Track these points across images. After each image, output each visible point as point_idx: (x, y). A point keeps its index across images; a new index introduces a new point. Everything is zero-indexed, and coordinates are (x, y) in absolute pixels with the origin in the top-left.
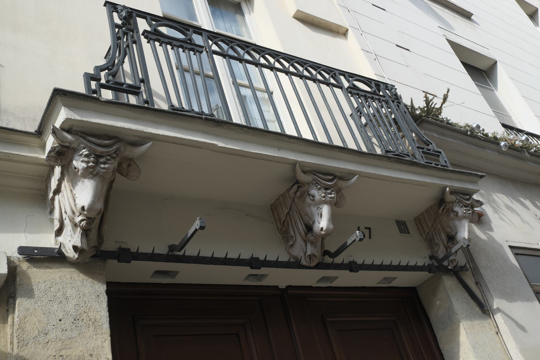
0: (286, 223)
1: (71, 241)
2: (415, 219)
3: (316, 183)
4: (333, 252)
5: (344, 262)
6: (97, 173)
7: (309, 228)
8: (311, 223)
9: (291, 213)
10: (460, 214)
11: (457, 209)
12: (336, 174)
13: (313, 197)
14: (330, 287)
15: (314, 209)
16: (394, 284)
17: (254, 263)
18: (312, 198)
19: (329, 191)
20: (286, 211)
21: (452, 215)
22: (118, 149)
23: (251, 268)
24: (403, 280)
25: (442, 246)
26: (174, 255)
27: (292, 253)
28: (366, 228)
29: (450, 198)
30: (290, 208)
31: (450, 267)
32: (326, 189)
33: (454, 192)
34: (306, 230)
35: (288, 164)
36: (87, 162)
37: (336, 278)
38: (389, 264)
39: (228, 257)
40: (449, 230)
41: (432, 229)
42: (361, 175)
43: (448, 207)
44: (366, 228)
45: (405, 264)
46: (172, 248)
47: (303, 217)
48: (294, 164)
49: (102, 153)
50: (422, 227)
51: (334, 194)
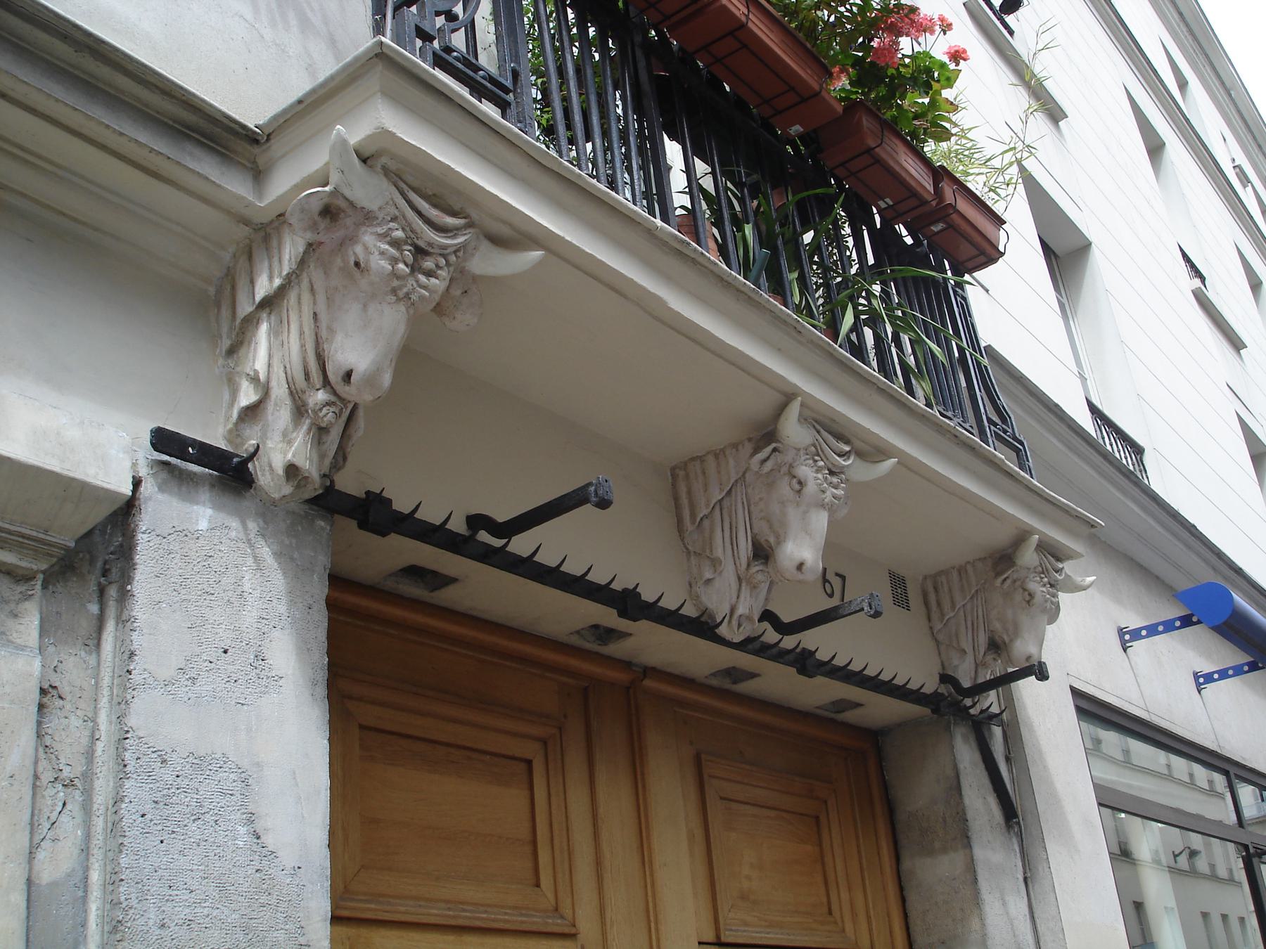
0: (706, 523)
1: (282, 448)
2: (925, 578)
3: (816, 453)
4: (786, 621)
5: (613, 586)
6: (407, 295)
7: (763, 553)
8: (772, 540)
9: (726, 503)
10: (811, 488)
11: (806, 471)
12: (475, 215)
13: (800, 483)
14: (597, 653)
15: (793, 514)
16: (850, 716)
17: (628, 603)
18: (797, 487)
19: (835, 480)
20: (717, 496)
21: (1018, 597)
22: (463, 247)
23: (620, 615)
24: (880, 710)
25: (970, 659)
26: (484, 539)
27: (704, 599)
28: (837, 575)
29: (794, 431)
30: (729, 492)
31: (972, 711)
32: (832, 473)
33: (830, 428)
34: (751, 554)
35: (779, 391)
36: (394, 261)
37: (753, 675)
38: (554, 565)
39: (536, 559)
40: (997, 626)
41: (962, 613)
42: (906, 463)
43: (1015, 576)
44: (837, 575)
45: (578, 572)
46: (477, 522)
47: (754, 520)
48: (788, 396)
49: (430, 245)
50: (939, 604)
51: (843, 489)
